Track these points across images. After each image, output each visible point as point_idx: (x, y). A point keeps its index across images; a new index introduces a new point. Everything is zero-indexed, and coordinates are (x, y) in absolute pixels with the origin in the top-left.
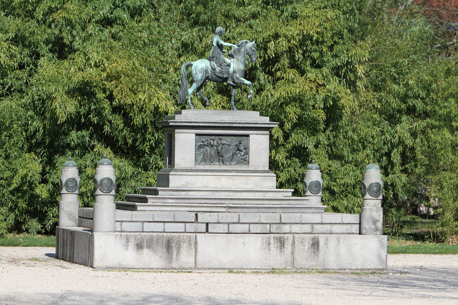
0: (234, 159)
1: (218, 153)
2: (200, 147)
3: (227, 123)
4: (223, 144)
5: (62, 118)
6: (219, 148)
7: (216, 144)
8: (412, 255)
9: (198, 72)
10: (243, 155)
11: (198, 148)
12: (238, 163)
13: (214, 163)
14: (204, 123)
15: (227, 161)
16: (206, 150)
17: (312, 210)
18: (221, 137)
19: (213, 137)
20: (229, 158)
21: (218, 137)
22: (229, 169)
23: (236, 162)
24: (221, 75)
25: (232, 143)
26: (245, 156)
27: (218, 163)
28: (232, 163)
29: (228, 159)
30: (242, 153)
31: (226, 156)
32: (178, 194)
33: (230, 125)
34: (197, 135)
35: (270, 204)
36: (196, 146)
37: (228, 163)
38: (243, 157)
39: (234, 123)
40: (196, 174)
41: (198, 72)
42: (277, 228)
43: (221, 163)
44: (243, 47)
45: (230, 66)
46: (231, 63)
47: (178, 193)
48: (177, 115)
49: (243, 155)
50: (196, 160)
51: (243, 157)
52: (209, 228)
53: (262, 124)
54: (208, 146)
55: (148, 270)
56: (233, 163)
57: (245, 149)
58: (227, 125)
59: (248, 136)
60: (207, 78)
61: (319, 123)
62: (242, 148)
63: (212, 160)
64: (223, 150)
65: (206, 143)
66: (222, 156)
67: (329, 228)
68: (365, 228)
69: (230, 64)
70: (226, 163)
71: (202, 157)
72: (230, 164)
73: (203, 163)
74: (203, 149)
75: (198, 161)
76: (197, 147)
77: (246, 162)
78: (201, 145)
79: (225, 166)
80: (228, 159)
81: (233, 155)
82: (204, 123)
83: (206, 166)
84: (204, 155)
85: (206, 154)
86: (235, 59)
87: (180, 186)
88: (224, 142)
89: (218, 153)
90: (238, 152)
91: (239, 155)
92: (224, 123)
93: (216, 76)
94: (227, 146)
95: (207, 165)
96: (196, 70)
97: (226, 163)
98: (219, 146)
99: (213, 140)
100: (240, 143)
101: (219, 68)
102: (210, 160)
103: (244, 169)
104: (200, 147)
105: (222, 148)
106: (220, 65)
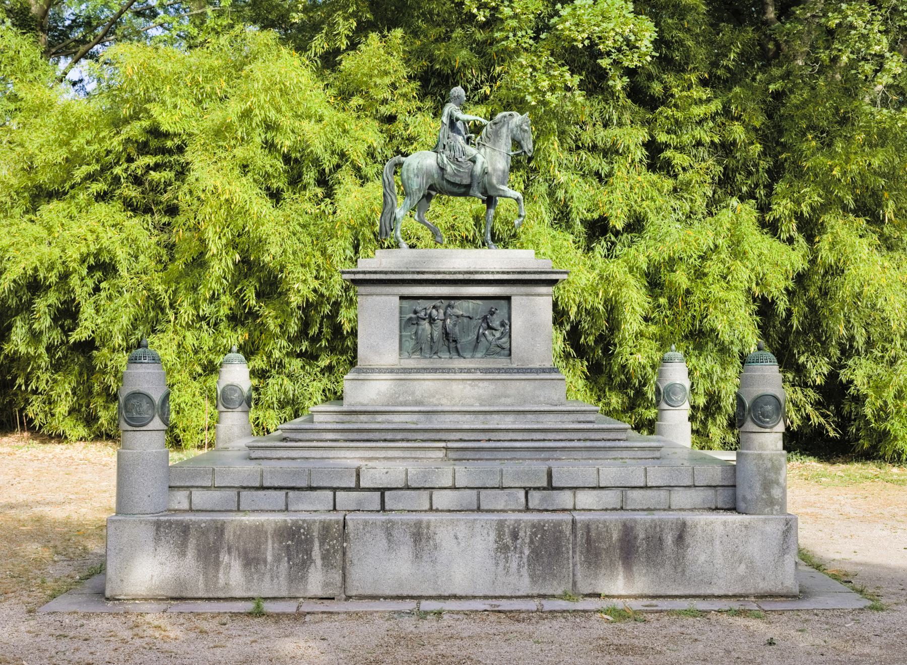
3: (460, 273)
4: (458, 317)
9: (412, 176)
12: (489, 353)
14: (413, 273)
17: (633, 453)
19: (437, 303)
21: (446, 302)
22: (471, 366)
24: (457, 180)
27: (447, 355)
32: (354, 420)
33: (467, 277)
34: (402, 298)
35: (544, 440)
36: (401, 321)
39: (476, 273)
40: (538, 377)
41: (412, 176)
42: (543, 500)
44: (503, 125)
45: (474, 162)
46: (479, 156)
47: (354, 418)
52: (386, 499)
53: (535, 273)
56: (479, 355)
58: (460, 277)
59: (508, 299)
60: (431, 187)
61: (128, 140)
62: (496, 323)
63: (435, 349)
67: (662, 497)
68: (744, 498)
69: (475, 157)
70: (465, 355)
72: (472, 357)
76: (403, 322)
78: (410, 319)
79: (462, 360)
81: (477, 338)
82: (413, 273)
86: (488, 150)
87: (365, 402)
92: (455, 273)
93: (448, 181)
94: (465, 320)
96: (408, 170)
97: (465, 355)
100: (492, 313)
101: (453, 166)
103: (501, 366)
106: (455, 161)
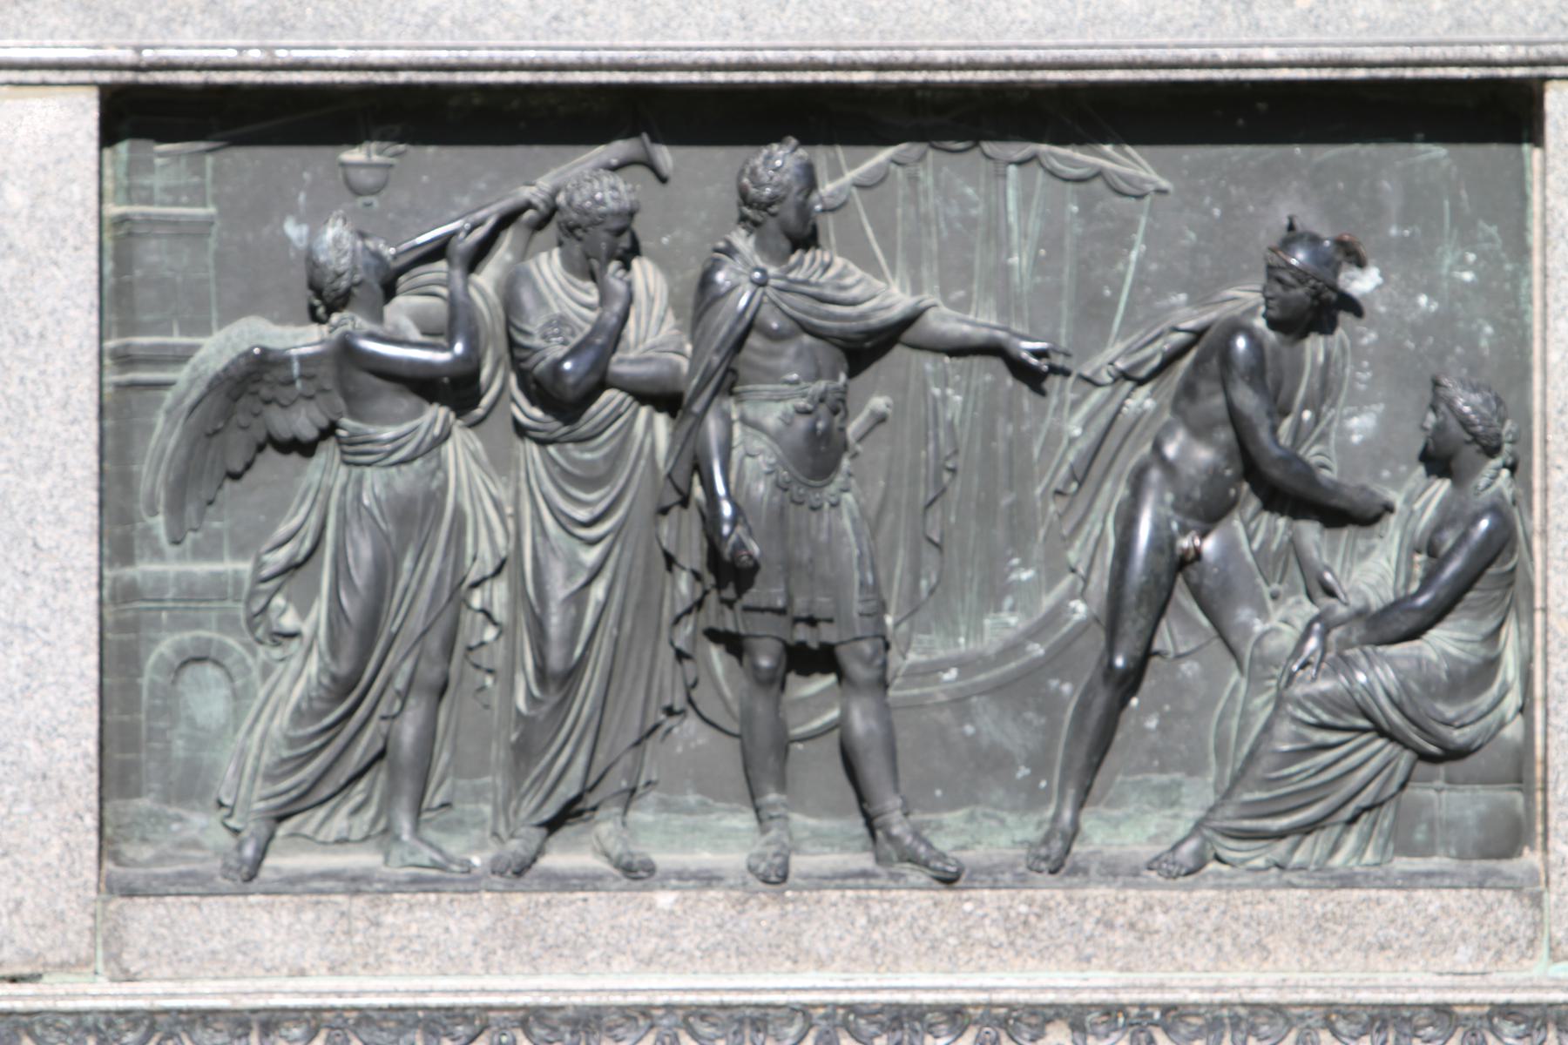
0: (1144, 716)
1: (728, 571)
2: (250, 419)
4: (865, 348)
5: (1000, 876)
6: (753, 442)
7: (655, 336)
8: (96, 522)
10: (1397, 624)
11: (205, 440)
12: (1278, 815)
13: (651, 831)
15: (978, 775)
16: (418, 515)
18: (780, 161)
19: (585, 175)
20: (1019, 687)
21: (703, 174)
23: (1198, 796)
25: (1094, 312)
26: (1445, 642)
27: (730, 838)
28: (1103, 834)
29: (989, 725)
30: (1374, 570)
31: (938, 653)
37: (1004, 836)
38: (1378, 674)
43: (825, 842)
48: (94, 114)
49: (1397, 624)
50: (129, 755)
51: (1378, 674)
54: (456, 390)
55: (838, 882)
56: (1125, 829)
57: (1437, 461)
62: (1354, 432)
64: (847, 502)
65: (402, 332)
66: (821, 660)
70: (951, 833)
71: (300, 675)
72: (1057, 859)
73: (326, 844)
74: (325, 468)
75: (191, 786)
76: (163, 435)
77: (1455, 801)
78: (255, 376)
79: (915, 901)
80: (989, 725)
83: (410, 916)
84: (362, 634)
85: (411, 612)
88: (891, 298)
89: (728, 571)
90: (1252, 530)
91: (1280, 623)
94: (956, 392)
95: (438, 879)
97: (951, 833)
98: (728, 382)
99: (606, 244)
100: (1316, 309)
102: (524, 752)
104: (250, 419)
105: (820, 453)
